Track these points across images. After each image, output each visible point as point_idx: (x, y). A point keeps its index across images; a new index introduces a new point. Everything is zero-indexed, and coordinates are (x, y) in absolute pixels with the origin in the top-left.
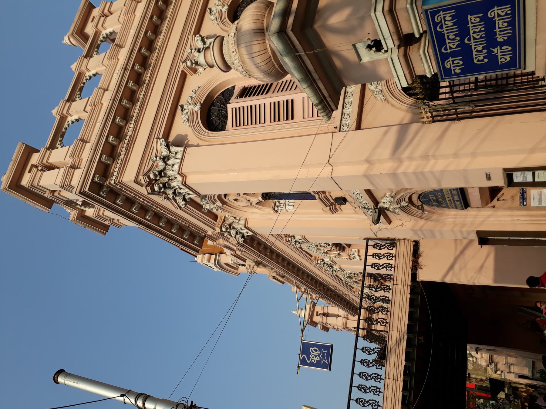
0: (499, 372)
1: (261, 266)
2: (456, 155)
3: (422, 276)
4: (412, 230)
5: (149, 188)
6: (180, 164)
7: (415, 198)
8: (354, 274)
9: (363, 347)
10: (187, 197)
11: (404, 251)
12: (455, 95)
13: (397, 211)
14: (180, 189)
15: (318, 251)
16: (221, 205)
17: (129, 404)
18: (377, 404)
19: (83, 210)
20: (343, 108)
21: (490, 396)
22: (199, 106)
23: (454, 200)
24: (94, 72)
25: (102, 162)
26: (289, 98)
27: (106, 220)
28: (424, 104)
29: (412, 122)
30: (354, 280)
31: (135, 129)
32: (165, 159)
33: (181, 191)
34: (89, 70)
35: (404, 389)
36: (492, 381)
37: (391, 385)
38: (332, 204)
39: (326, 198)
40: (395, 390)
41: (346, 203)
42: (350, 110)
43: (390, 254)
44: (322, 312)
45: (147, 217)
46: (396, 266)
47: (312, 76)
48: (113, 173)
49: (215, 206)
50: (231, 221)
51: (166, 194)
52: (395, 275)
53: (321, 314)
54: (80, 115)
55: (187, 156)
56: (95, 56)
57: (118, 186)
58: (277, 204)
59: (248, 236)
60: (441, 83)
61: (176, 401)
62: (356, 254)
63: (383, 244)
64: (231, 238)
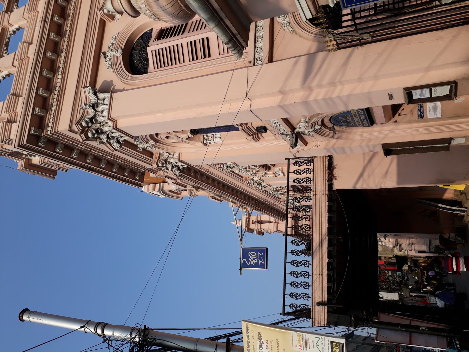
0: (403, 251)
1: (200, 190)
2: (360, 79)
3: (337, 185)
4: (325, 149)
5: (83, 135)
6: (109, 110)
7: (326, 121)
8: (280, 188)
9: (292, 261)
10: (121, 140)
11: (320, 167)
12: (357, 21)
13: (311, 134)
14: (113, 133)
15: (248, 173)
16: (154, 143)
17: (89, 333)
18: (307, 296)
19: (29, 159)
20: (255, 42)
21: (396, 268)
22: (120, 51)
23: (361, 119)
24: (16, 26)
25: (36, 115)
26: (204, 36)
27: (53, 166)
28: (329, 33)
29: (319, 50)
30: (280, 192)
31: (63, 80)
32: (94, 106)
33: (114, 135)
34: (11, 25)
35: (329, 281)
36: (397, 257)
37: (317, 279)
38: (254, 133)
39: (249, 128)
40: (321, 283)
41: (266, 131)
42: (262, 44)
43: (309, 169)
44: (256, 220)
45: (88, 161)
46: (315, 179)
47: (218, 15)
48: (48, 124)
49: (148, 145)
50: (166, 157)
51: (101, 139)
52: (314, 187)
53: (255, 222)
54: (10, 70)
55: (114, 102)
56: (15, 10)
57: (55, 136)
58: (206, 137)
59: (183, 168)
60: (343, 11)
61: (131, 326)
62: (280, 172)
63: (302, 161)
64: (168, 172)
